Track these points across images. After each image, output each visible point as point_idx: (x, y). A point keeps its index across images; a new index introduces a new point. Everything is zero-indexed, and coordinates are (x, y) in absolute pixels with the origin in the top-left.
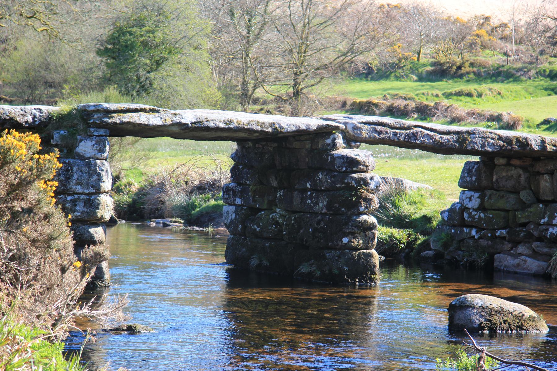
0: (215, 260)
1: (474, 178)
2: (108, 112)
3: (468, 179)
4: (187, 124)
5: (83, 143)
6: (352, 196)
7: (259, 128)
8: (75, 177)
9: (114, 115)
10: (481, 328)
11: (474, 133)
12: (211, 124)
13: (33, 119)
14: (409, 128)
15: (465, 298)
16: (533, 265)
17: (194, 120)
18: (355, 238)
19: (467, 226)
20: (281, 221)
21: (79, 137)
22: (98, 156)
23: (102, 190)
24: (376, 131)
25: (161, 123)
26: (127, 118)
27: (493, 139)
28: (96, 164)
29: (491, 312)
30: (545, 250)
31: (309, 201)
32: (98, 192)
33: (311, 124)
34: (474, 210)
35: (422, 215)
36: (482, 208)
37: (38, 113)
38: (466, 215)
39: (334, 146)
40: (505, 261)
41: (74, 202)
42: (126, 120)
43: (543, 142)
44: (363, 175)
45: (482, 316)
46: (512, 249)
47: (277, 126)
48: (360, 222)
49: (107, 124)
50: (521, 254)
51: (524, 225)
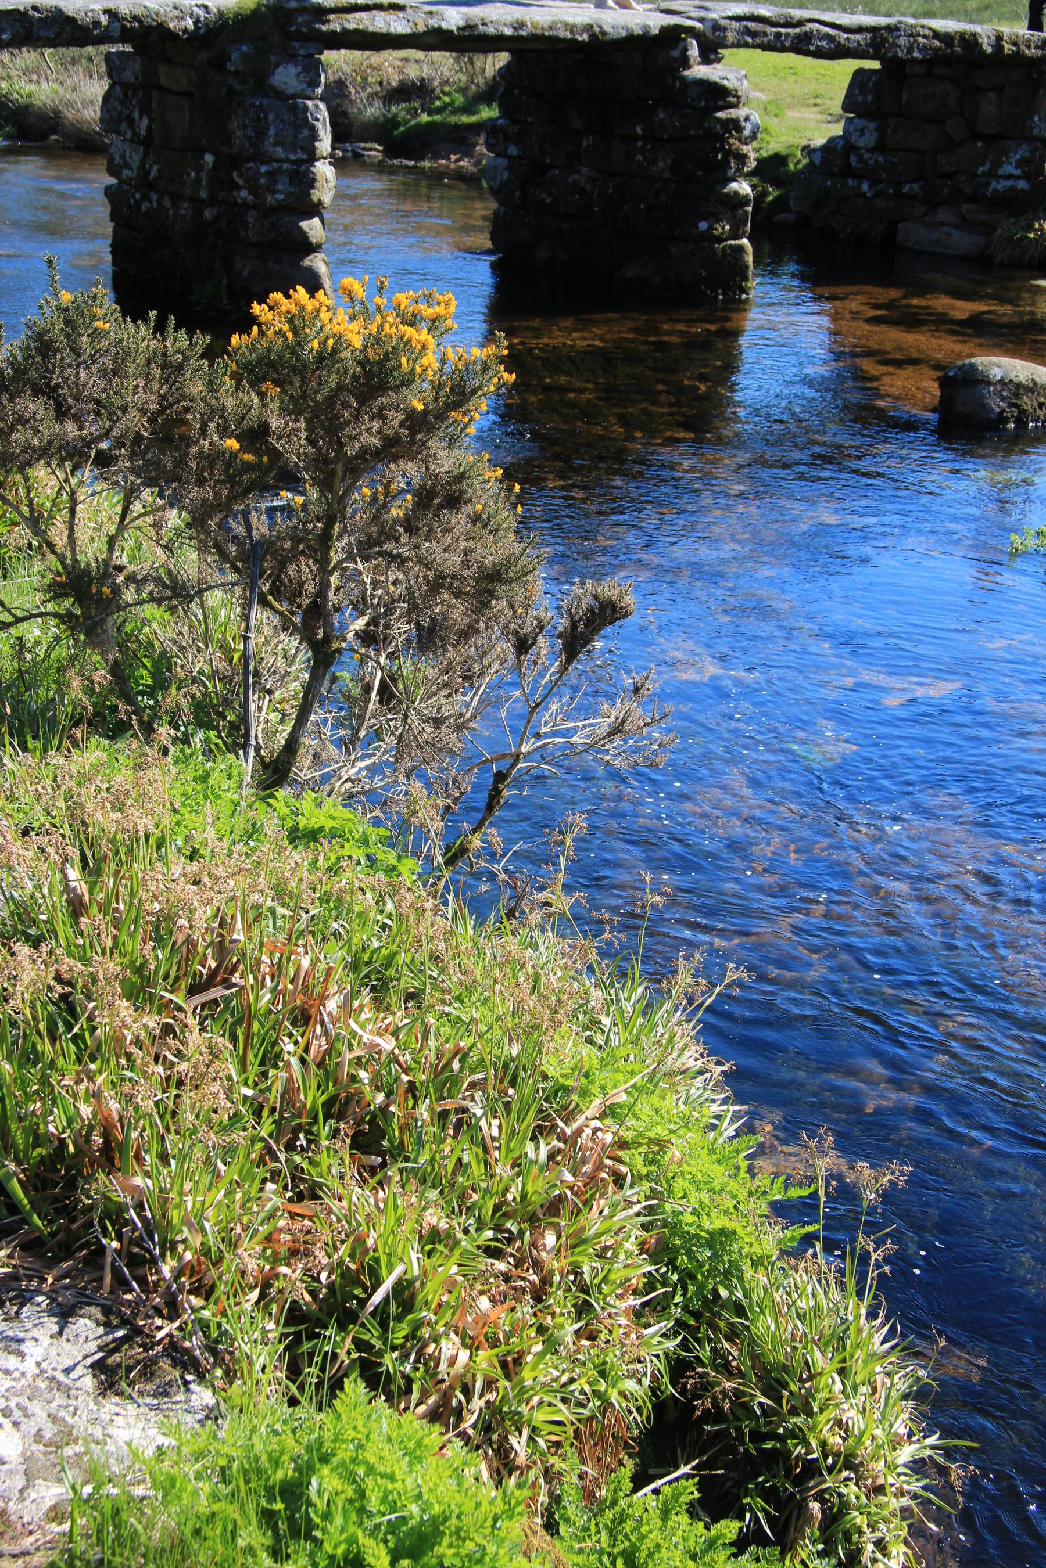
0: (470, 240)
1: (870, 98)
2: (321, 13)
3: (860, 99)
4: (451, 32)
5: (281, 69)
6: (718, 150)
7: (568, 35)
8: (272, 131)
9: (332, 17)
10: (1002, 419)
11: (897, 29)
12: (491, 30)
13: (195, 24)
14: (800, 23)
15: (972, 366)
16: (963, 241)
17: (462, 23)
18: (718, 221)
19: (854, 177)
20: (589, 188)
21: (273, 58)
22: (309, 92)
23: (318, 154)
24: (748, 31)
25: (408, 31)
26: (354, 22)
27: (925, 37)
28: (306, 108)
29: (1018, 389)
30: (983, 217)
31: (640, 157)
32: (313, 157)
33: (651, 23)
34: (868, 150)
35: (771, 153)
36: (880, 147)
37: (201, 13)
38: (853, 159)
39: (686, 63)
40: (916, 233)
41: (272, 175)
42: (351, 26)
43: (999, 38)
44: (733, 113)
45: (1003, 399)
46: (926, 214)
47: (597, 29)
48: (728, 195)
49: (319, 31)
50: (942, 224)
51: (949, 175)
